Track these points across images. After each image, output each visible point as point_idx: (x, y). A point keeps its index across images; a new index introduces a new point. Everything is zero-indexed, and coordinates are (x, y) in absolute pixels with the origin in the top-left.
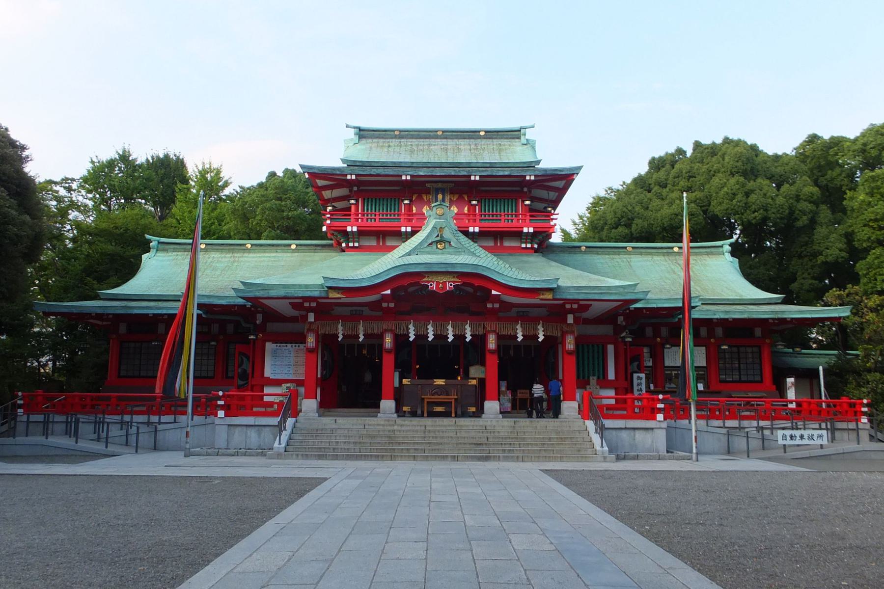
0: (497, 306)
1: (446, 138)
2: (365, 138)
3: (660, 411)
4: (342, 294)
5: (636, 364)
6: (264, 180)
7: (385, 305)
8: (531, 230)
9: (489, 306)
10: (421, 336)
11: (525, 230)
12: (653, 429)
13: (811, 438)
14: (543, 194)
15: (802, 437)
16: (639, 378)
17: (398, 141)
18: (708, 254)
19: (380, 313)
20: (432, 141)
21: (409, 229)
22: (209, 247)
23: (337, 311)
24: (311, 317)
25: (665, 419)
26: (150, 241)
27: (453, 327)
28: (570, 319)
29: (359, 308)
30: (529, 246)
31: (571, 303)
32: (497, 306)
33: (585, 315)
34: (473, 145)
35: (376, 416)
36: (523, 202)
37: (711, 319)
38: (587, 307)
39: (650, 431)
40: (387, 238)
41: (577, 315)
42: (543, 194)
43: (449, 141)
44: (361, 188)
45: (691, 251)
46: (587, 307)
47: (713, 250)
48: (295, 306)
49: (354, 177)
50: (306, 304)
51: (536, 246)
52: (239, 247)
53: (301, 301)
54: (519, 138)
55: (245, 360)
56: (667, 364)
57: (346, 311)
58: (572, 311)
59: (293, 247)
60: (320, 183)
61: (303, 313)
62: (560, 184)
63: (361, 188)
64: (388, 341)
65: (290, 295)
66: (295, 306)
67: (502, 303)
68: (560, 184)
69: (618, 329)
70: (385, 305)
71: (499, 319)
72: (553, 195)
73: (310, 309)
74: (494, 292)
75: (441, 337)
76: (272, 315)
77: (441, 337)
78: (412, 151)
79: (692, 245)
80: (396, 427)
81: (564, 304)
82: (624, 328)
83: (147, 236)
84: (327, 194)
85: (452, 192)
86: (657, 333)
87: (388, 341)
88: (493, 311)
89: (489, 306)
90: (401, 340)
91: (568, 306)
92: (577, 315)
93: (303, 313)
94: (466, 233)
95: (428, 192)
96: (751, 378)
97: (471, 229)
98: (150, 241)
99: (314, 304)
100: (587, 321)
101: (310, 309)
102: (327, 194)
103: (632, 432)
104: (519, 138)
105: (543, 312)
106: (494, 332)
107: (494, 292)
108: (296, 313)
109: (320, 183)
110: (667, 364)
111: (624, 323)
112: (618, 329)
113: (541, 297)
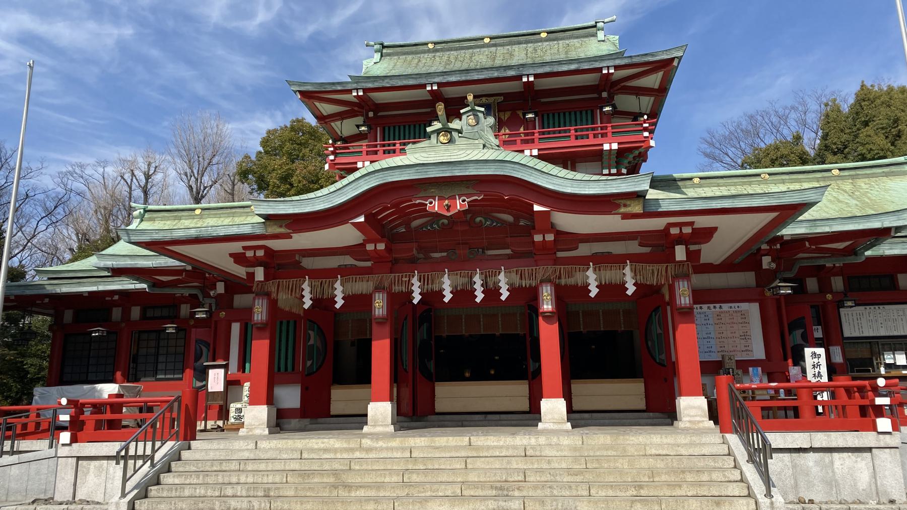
0: (550, 237)
1: (495, 45)
2: (388, 55)
3: (879, 411)
4: (287, 226)
5: (798, 333)
7: (370, 247)
8: (615, 146)
9: (538, 238)
10: (432, 297)
11: (606, 147)
12: (870, 449)
16: (814, 355)
17: (431, 55)
18: (887, 175)
19: (368, 264)
22: (206, 212)
24: (259, 274)
25: (895, 428)
27: (635, 272)
28: (680, 253)
32: (550, 237)
35: (672, 424)
36: (601, 108)
39: (867, 455)
46: (707, 234)
47: (893, 168)
48: (238, 258)
49: (361, 93)
52: (242, 210)
54: (595, 35)
55: (205, 350)
58: (681, 239)
60: (327, 109)
62: (653, 80)
64: (380, 306)
65: (204, 233)
66: (238, 258)
67: (559, 234)
68: (653, 80)
69: (765, 279)
70: (370, 247)
71: (557, 261)
72: (646, 102)
74: (537, 208)
75: (464, 294)
77: (464, 294)
82: (772, 275)
85: (501, 108)
86: (825, 287)
87: (380, 306)
89: (538, 238)
90: (400, 300)
99: (260, 253)
100: (710, 268)
103: (827, 456)
104: (595, 35)
106: (548, 281)
107: (537, 208)
110: (847, 333)
111: (774, 265)
112: (765, 279)
113: (623, 210)
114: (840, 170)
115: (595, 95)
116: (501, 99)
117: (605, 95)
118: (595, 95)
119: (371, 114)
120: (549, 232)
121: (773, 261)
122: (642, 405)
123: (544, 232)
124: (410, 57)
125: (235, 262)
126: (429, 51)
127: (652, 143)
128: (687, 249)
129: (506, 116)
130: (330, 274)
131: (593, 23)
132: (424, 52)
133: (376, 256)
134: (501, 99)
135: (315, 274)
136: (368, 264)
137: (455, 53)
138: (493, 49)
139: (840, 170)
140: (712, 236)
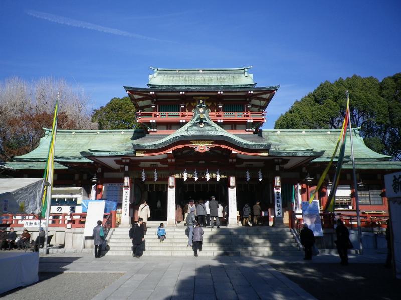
0: (234, 161)
1: (204, 74)
6: (121, 99)
7: (169, 161)
8: (252, 121)
9: (230, 161)
11: (248, 121)
13: (278, 202)
14: (257, 103)
15: (35, 224)
17: (178, 76)
19: (167, 166)
20: (197, 75)
21: (184, 121)
23: (142, 165)
24: (127, 168)
26: (45, 131)
27: (249, 172)
29: (155, 163)
30: (250, 130)
31: (126, 159)
32: (234, 161)
33: (287, 166)
34: (218, 77)
36: (247, 106)
37: (385, 170)
38: (286, 162)
40: (173, 127)
41: (281, 166)
42: (257, 103)
43: (206, 75)
44: (159, 100)
45: (57, 133)
46: (286, 162)
50: (124, 161)
51: (254, 130)
53: (120, 159)
54: (244, 73)
56: (336, 195)
57: (148, 165)
58: (278, 164)
59: (123, 133)
60: (137, 97)
61: (123, 166)
62: (266, 96)
63: (159, 100)
66: (118, 162)
68: (266, 96)
70: (169, 161)
72: (262, 103)
73: (126, 164)
76: (106, 169)
78: (186, 81)
79: (58, 131)
80: (175, 234)
81: (274, 159)
83: (43, 129)
84: (140, 104)
85: (208, 101)
88: (232, 164)
89: (230, 161)
91: (276, 161)
92: (281, 166)
93: (123, 166)
94: (216, 123)
95: (194, 101)
96: (376, 203)
97: (218, 121)
98: (45, 131)
99: (128, 161)
101: (126, 164)
102: (140, 104)
104: (244, 73)
105: (262, 164)
108: (117, 167)
109: (137, 97)
110: (336, 195)
114: (331, 132)
115: (244, 99)
116: (208, 98)
117: (248, 100)
118: (244, 99)
119: (155, 100)
120: (234, 159)
121: (306, 169)
122: (51, 213)
123: (232, 159)
124: (169, 76)
125: (116, 163)
126: (177, 74)
127: (265, 121)
128: (280, 167)
129: (209, 105)
130: (152, 169)
131: (243, 69)
132: (175, 74)
133: (171, 164)
134: (208, 98)
135: (147, 169)
136: (167, 166)
137: (188, 76)
138: (203, 75)
139: (331, 132)
140: (287, 163)
